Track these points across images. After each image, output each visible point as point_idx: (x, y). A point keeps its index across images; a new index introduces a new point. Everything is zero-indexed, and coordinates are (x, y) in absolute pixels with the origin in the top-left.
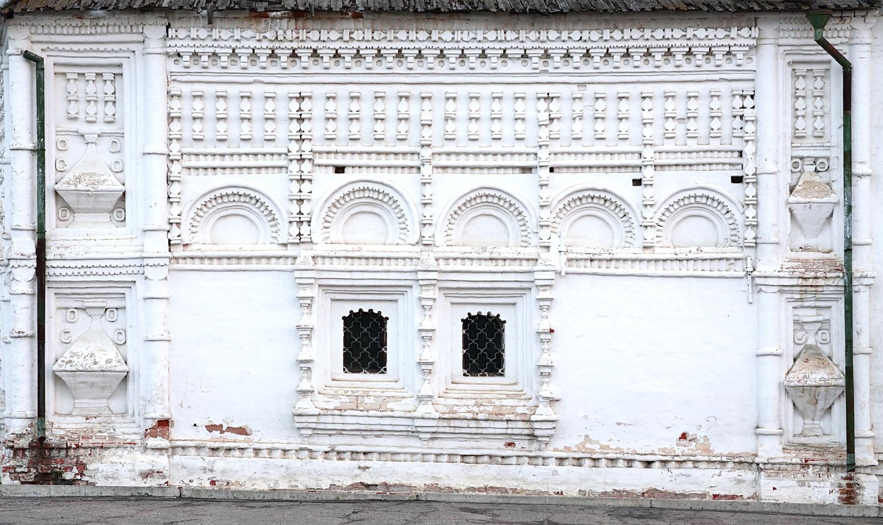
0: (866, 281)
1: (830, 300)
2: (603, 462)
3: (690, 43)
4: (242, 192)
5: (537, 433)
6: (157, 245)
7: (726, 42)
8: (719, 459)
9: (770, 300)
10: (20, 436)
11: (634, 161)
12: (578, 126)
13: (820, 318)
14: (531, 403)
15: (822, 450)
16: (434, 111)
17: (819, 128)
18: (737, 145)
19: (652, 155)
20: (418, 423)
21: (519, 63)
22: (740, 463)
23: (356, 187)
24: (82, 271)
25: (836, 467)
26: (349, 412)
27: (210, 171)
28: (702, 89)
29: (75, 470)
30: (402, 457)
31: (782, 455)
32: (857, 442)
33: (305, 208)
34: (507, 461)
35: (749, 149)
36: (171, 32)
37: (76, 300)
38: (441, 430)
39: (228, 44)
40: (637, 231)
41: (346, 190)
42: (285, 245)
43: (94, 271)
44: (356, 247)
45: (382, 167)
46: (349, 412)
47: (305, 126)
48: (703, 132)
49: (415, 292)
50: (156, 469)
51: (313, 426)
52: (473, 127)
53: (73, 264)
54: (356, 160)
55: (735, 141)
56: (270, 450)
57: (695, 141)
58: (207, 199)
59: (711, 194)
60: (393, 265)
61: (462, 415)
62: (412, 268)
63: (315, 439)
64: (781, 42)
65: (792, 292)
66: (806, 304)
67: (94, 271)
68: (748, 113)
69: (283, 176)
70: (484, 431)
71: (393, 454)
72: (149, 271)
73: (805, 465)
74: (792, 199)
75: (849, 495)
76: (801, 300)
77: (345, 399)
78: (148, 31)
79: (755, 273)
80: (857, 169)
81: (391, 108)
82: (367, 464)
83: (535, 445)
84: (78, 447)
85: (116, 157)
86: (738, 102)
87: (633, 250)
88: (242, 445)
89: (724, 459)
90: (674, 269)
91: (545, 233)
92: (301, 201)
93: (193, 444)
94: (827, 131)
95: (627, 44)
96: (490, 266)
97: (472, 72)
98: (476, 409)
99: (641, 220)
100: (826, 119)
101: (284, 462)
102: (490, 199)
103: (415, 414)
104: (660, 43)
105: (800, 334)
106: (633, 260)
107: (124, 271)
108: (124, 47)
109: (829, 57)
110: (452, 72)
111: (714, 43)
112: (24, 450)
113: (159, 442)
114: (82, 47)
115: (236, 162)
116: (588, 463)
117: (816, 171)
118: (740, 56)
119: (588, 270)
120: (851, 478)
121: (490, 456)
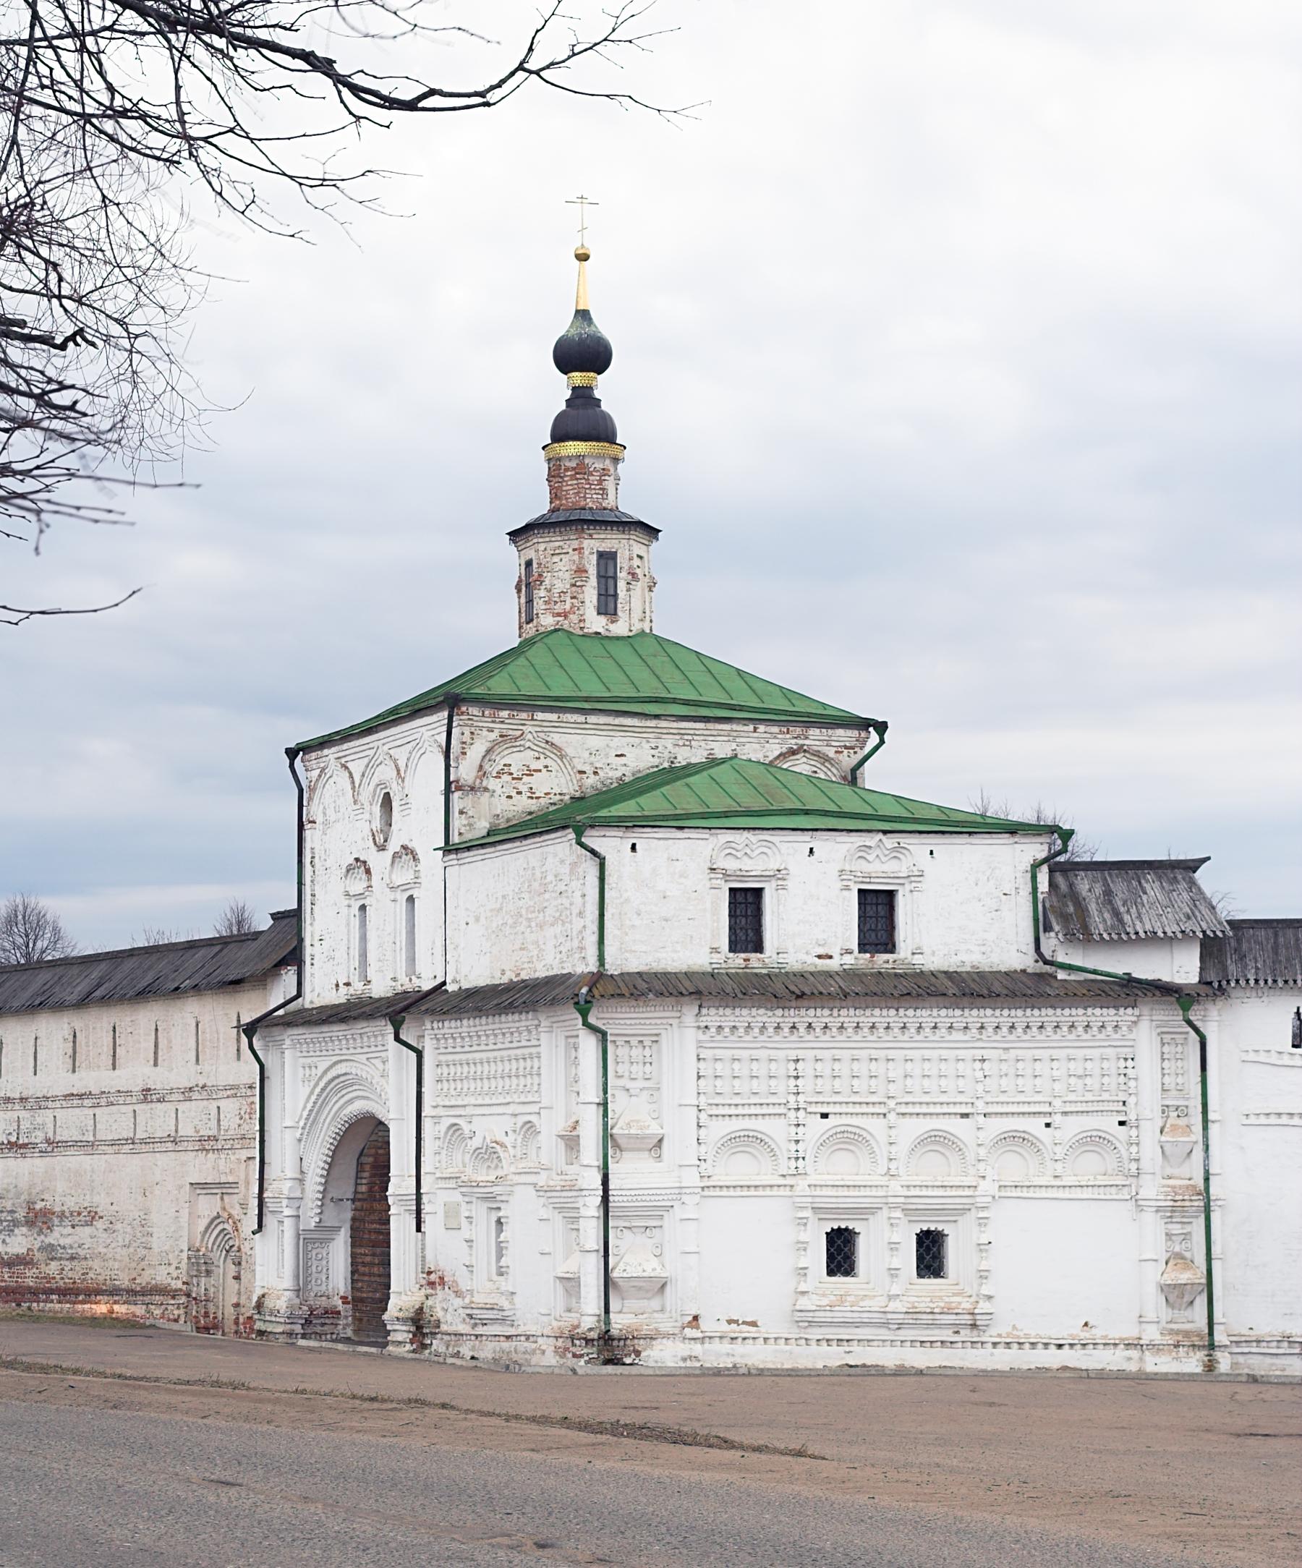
0: (1219, 1203)
1: (1192, 1217)
2: (1027, 1346)
3: (1089, 1019)
4: (751, 1134)
5: (978, 1323)
6: (691, 1179)
7: (1054, 1019)
8: (1112, 1342)
9: (1149, 1217)
10: (590, 1330)
11: (1046, 1109)
12: (1004, 1081)
13: (1185, 1231)
14: (973, 1299)
15: (1187, 1334)
16: (895, 1071)
17: (1180, 1083)
18: (1122, 1097)
19: (1060, 1104)
20: (890, 1316)
21: (961, 1032)
22: (1129, 1344)
23: (839, 1130)
24: (634, 1199)
25: (1199, 1346)
26: (837, 1308)
27: (727, 1118)
28: (1095, 1053)
29: (633, 1356)
30: (875, 1343)
31: (1159, 1337)
32: (1216, 1327)
33: (801, 1146)
34: (954, 1345)
35: (1131, 1101)
36: (704, 1011)
37: (625, 1221)
38: (906, 1321)
39: (746, 1019)
40: (1049, 1163)
41: (830, 1133)
42: (784, 1176)
43: (644, 1198)
44: (839, 1177)
45: (857, 1114)
46: (837, 1308)
47: (800, 1082)
48: (1097, 1086)
49: (885, 1213)
50: (693, 1354)
51: (810, 1319)
52: (926, 1082)
53: (628, 1193)
54: (838, 1109)
55: (1120, 1093)
56: (776, 1339)
57: (1091, 1093)
58: (725, 1140)
59: (1103, 1135)
60: (867, 1192)
61: (923, 1310)
62: (884, 1194)
63: (809, 1330)
64: (1154, 1018)
65: (1165, 1211)
66: (1174, 1220)
67: (644, 1198)
68: (1129, 1071)
69: (782, 1120)
70: (938, 1322)
71: (868, 1341)
72: (685, 1198)
73: (1176, 1346)
74: (1163, 1139)
75: (1210, 1366)
76: (1171, 1217)
77: (833, 1298)
78: (685, 1009)
79: (1138, 1197)
80: (1211, 1116)
81: (862, 1068)
82: (851, 1349)
83: (975, 1332)
84: (634, 1337)
85: (654, 1106)
86: (1122, 1063)
87: (969, 1178)
88: (755, 1335)
89: (1117, 1342)
90: (1078, 1193)
91: (981, 1166)
92: (797, 1142)
93: (718, 1334)
94: (1186, 1085)
95: (1042, 1019)
96: (941, 1192)
97: (926, 1040)
98: (932, 1305)
99: (1052, 1155)
100: (1186, 1076)
101: (788, 1348)
102: (937, 1139)
103: (887, 1309)
104: (1067, 1019)
105: (1169, 1243)
106: (1047, 1187)
107: (665, 1198)
108: (664, 1021)
109: (1190, 1029)
110: (911, 1040)
111: (1106, 1019)
112: (593, 1340)
113: (689, 1332)
114: (633, 1022)
115: (746, 1111)
116: (1016, 1346)
117: (1178, 1116)
118: (1124, 1028)
119: (1014, 1194)
120: (1211, 1355)
121: (942, 1342)
